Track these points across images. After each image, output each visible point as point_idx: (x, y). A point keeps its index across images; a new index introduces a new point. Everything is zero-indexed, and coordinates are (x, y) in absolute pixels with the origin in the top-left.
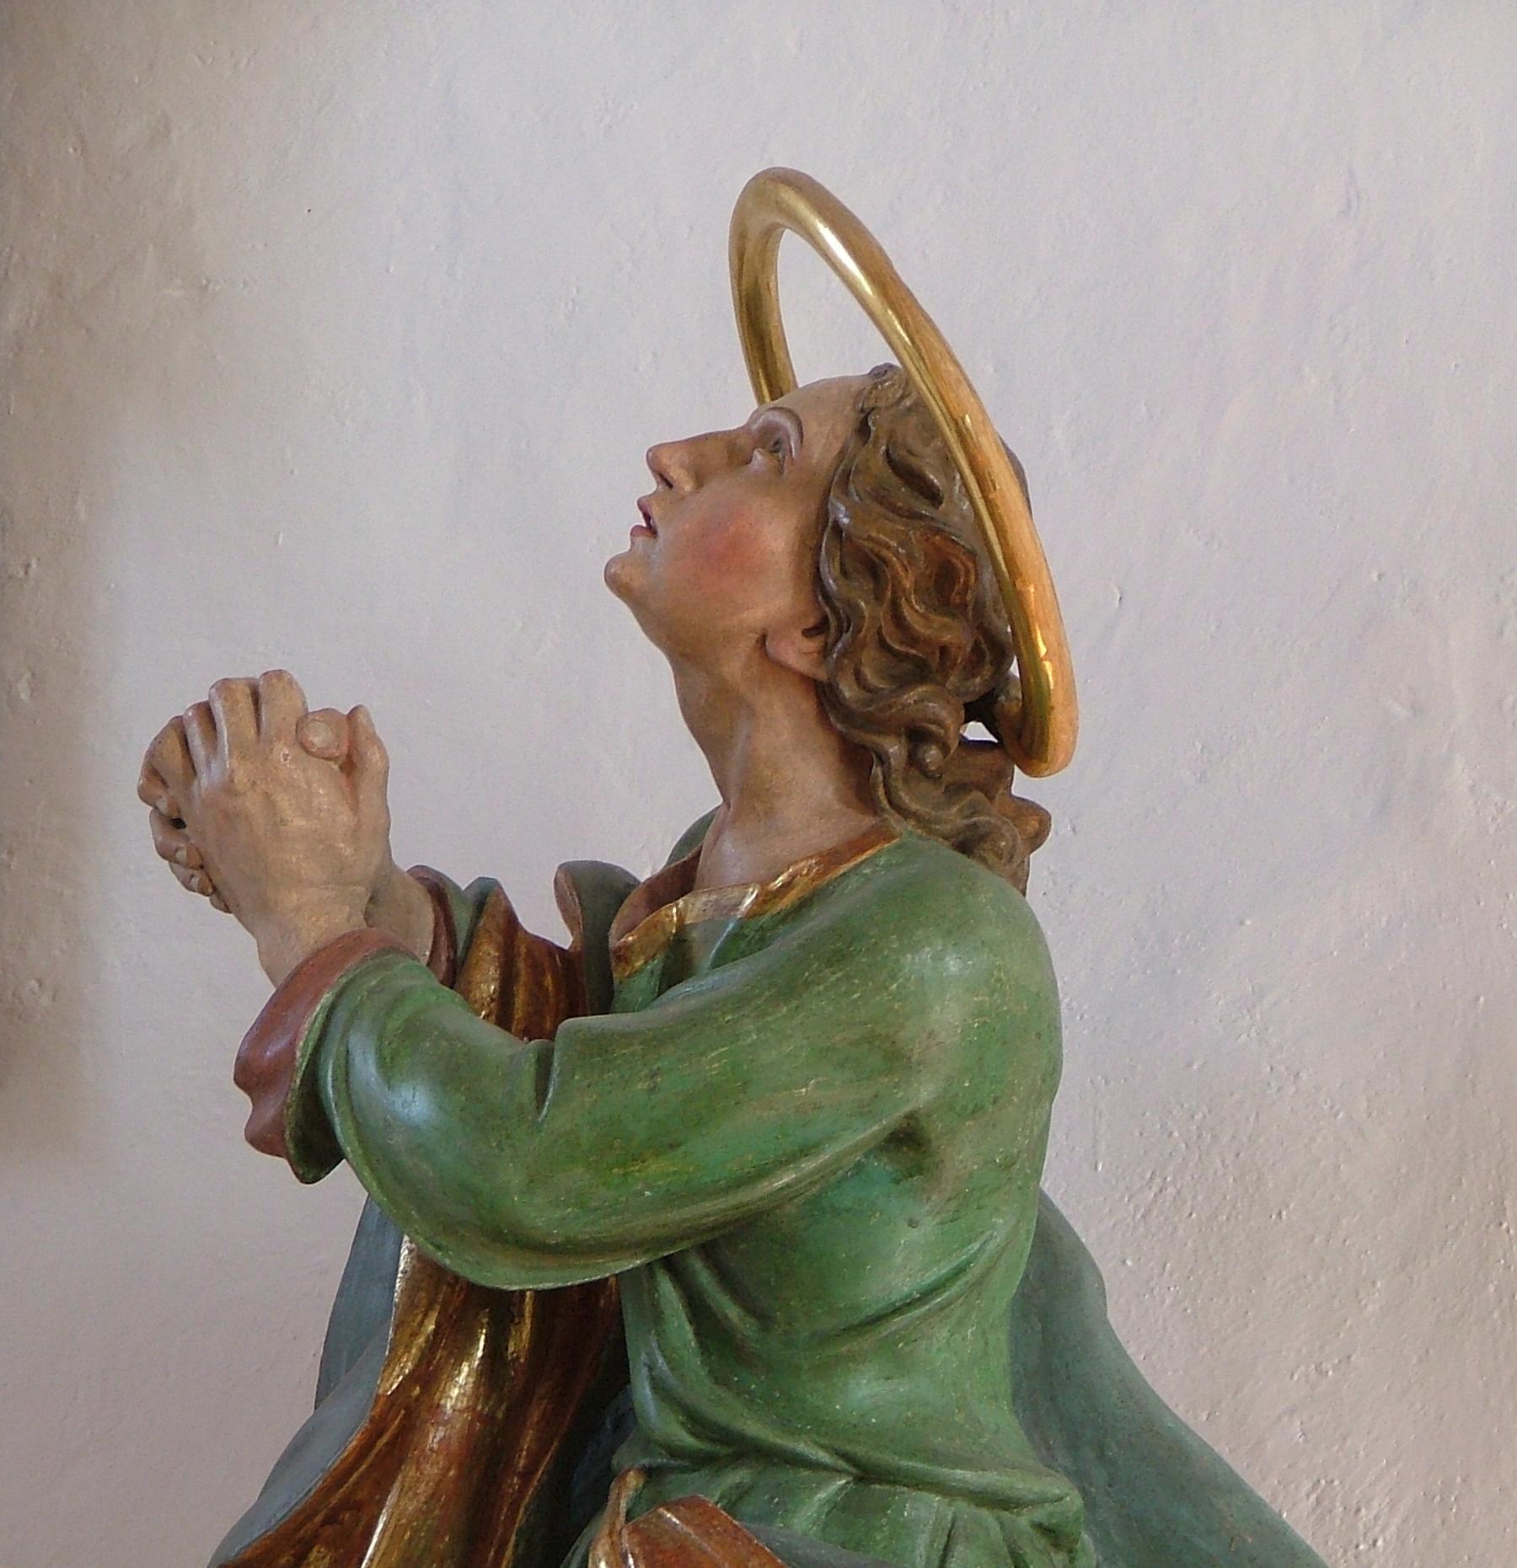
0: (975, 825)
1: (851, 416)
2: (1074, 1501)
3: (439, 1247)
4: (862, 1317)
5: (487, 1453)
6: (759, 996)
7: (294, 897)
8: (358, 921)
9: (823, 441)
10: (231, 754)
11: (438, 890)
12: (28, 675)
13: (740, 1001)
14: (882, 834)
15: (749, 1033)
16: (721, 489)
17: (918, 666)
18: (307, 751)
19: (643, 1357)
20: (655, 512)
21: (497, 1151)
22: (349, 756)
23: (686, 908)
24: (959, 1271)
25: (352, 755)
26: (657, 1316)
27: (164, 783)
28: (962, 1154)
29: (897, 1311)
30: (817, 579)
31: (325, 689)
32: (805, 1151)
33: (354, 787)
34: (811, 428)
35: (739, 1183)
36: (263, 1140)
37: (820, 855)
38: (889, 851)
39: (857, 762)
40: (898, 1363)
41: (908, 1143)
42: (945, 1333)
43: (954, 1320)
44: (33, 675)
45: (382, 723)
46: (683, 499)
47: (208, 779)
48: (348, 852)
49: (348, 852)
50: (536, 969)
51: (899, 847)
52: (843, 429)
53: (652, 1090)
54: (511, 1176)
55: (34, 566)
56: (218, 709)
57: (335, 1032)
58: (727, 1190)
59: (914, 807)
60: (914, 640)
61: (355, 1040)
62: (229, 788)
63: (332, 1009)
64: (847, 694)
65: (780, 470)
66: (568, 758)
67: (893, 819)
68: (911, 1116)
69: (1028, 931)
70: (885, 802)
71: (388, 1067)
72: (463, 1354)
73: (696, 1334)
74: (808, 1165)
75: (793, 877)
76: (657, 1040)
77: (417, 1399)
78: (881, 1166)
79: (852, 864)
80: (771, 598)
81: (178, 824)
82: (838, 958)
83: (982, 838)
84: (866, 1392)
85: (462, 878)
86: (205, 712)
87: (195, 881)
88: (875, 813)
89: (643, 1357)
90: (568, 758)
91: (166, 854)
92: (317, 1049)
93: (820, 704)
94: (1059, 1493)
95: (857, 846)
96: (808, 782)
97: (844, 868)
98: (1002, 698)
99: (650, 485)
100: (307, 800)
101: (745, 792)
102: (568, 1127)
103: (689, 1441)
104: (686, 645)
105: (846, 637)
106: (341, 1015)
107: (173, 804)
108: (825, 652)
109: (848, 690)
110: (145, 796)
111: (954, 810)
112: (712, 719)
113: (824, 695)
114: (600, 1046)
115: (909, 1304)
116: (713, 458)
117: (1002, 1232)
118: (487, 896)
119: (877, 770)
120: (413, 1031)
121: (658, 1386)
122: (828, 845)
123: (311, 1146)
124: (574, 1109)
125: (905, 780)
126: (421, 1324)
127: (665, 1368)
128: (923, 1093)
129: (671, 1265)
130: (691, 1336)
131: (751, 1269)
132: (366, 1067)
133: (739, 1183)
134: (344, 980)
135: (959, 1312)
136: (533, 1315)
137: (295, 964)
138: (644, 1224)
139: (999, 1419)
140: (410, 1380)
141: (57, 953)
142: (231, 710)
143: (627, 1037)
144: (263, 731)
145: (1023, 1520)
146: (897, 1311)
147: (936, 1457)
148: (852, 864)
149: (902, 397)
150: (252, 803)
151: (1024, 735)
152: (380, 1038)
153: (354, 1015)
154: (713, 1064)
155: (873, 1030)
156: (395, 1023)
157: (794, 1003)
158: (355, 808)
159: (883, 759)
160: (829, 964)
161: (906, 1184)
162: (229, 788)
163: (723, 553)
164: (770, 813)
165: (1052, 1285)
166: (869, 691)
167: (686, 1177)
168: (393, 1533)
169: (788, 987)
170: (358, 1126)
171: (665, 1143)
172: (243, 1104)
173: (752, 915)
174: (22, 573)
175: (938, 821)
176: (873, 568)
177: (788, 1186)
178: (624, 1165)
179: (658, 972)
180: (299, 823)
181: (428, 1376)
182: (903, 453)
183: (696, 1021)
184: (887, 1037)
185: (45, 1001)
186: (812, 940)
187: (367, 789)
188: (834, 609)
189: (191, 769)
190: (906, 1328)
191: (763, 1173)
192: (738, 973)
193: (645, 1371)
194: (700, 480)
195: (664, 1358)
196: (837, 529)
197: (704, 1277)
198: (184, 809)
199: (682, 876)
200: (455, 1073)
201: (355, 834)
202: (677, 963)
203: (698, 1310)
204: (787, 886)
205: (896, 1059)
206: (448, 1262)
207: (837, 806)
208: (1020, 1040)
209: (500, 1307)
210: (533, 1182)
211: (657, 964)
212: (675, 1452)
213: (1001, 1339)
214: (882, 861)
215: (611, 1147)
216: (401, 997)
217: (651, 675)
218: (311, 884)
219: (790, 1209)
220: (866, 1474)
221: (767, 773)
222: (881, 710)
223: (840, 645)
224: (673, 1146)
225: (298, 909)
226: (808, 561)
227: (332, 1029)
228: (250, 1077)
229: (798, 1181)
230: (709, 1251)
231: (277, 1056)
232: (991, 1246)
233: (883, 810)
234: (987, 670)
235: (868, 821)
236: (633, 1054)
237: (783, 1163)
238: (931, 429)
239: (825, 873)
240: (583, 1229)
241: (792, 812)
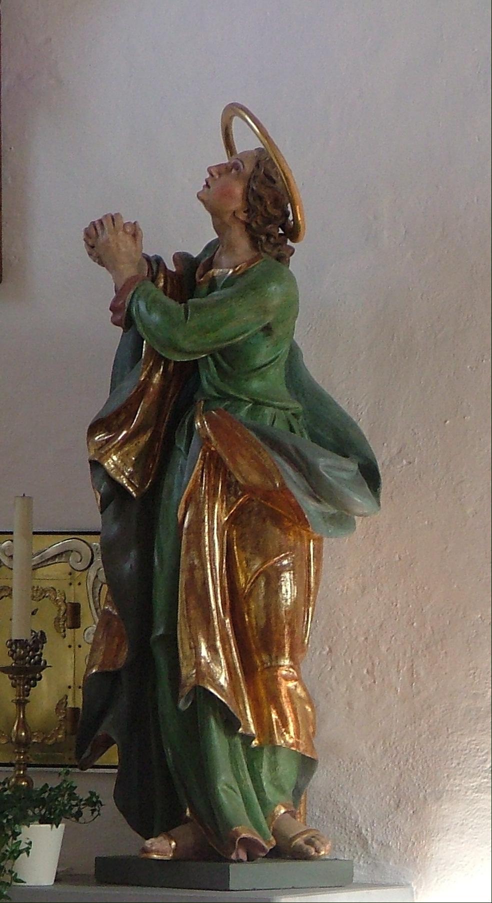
1: (255, 161)
2: (301, 409)
5: (163, 391)
9: (248, 168)
11: (148, 259)
17: (269, 220)
20: (210, 183)
24: (277, 357)
25: (135, 234)
26: (208, 368)
28: (279, 332)
30: (247, 200)
39: (254, 241)
40: (263, 377)
41: (268, 330)
45: (141, 225)
47: (102, 239)
50: (172, 280)
52: (253, 165)
54: (179, 336)
57: (135, 300)
60: (269, 213)
61: (140, 302)
66: (183, 229)
69: (292, 278)
71: (149, 310)
78: (262, 334)
80: (236, 204)
84: (256, 385)
86: (101, 221)
91: (90, 255)
92: (131, 302)
94: (296, 406)
96: (242, 245)
99: (208, 176)
100: (125, 244)
103: (216, 394)
104: (215, 214)
106: (136, 296)
108: (248, 217)
109: (254, 225)
113: (248, 226)
115: (265, 365)
116: (223, 170)
117: (285, 348)
118: (159, 261)
120: (154, 301)
124: (194, 322)
128: (269, 319)
131: (233, 359)
132: (143, 308)
138: (209, 347)
139: (283, 389)
140: (146, 376)
145: (289, 412)
147: (273, 400)
151: (293, 233)
159: (261, 241)
162: (108, 241)
163: (226, 193)
165: (294, 353)
168: (142, 412)
176: (260, 198)
180: (124, 250)
181: (150, 376)
183: (220, 303)
186: (247, 284)
187: (138, 238)
192: (229, 291)
194: (220, 176)
195: (208, 377)
197: (219, 357)
200: (166, 312)
201: (136, 251)
202: (213, 285)
203: (217, 364)
205: (266, 312)
208: (290, 306)
209: (167, 362)
212: (210, 396)
220: (256, 403)
238: (274, 166)
241: (239, 251)
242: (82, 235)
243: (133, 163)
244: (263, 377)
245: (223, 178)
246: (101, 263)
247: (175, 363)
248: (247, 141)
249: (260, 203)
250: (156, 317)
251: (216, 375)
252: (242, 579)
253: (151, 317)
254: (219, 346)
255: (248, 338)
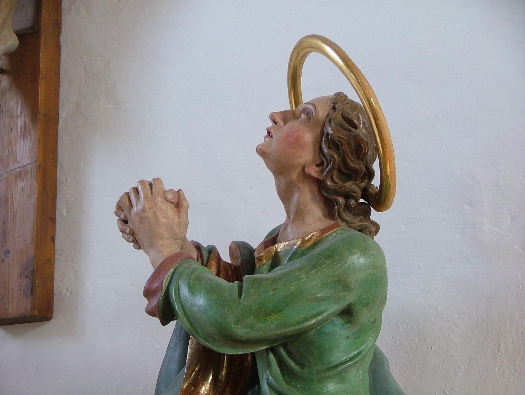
0: (362, 225)
1: (330, 105)
3: (207, 341)
4: (332, 365)
6: (306, 268)
7: (161, 242)
8: (179, 250)
10: (144, 200)
11: (198, 247)
12: (66, 208)
13: (300, 269)
14: (338, 225)
15: (303, 278)
16: (292, 125)
18: (166, 200)
19: (265, 377)
20: (272, 131)
21: (227, 312)
22: (178, 203)
23: (278, 247)
24: (360, 353)
25: (178, 203)
27: (123, 210)
28: (363, 316)
29: (342, 364)
30: (321, 149)
31: (170, 184)
32: (319, 314)
33: (179, 212)
34: (319, 108)
35: (299, 323)
36: (151, 313)
37: (320, 230)
38: (340, 230)
42: (355, 371)
43: (357, 367)
44: (68, 208)
45: (188, 195)
46: (281, 127)
48: (177, 230)
49: (177, 230)
50: (226, 269)
51: (343, 229)
53: (274, 295)
54: (231, 319)
55: (69, 179)
56: (140, 188)
58: (295, 325)
59: (346, 218)
61: (180, 282)
62: (143, 210)
63: (173, 274)
64: (329, 183)
65: (309, 119)
66: (242, 205)
67: (339, 221)
68: (349, 305)
70: (337, 216)
71: (192, 289)
72: (206, 379)
73: (281, 370)
74: (319, 318)
75: (312, 236)
76: (274, 280)
77: (193, 391)
78: (338, 321)
79: (329, 233)
80: (306, 156)
81: (126, 222)
82: (329, 257)
83: (366, 228)
85: (205, 244)
86: (136, 190)
87: (131, 239)
88: (334, 220)
89: (265, 377)
90: (242, 205)
91: (123, 231)
93: (319, 188)
95: (331, 228)
97: (327, 234)
98: (370, 189)
99: (270, 124)
101: (296, 215)
102: (249, 305)
105: (330, 166)
106: (176, 275)
107: (125, 216)
108: (322, 171)
110: (117, 214)
111: (357, 220)
112: (285, 194)
113: (320, 184)
114: (258, 281)
116: (286, 117)
118: (212, 250)
119: (336, 207)
120: (199, 279)
121: (269, 385)
122: (321, 228)
123: (165, 312)
125: (344, 211)
126: (195, 368)
127: (272, 380)
128: (350, 298)
129: (273, 350)
130: (279, 371)
132: (184, 291)
133: (299, 323)
134: (177, 265)
135: (359, 365)
136: (227, 367)
137: (161, 262)
141: (72, 282)
142: (144, 188)
143: (266, 279)
144: (153, 192)
146: (342, 364)
148: (329, 233)
149: (345, 100)
150: (150, 214)
152: (189, 280)
153: (180, 275)
154: (293, 287)
155: (340, 278)
156: (193, 277)
157: (316, 270)
158: (179, 218)
160: (327, 258)
161: (345, 326)
164: (303, 219)
166: (335, 183)
167: (283, 321)
169: (315, 265)
170: (182, 306)
171: (277, 310)
172: (145, 301)
173: (300, 247)
174: (65, 181)
175: (352, 223)
177: (314, 324)
178: (265, 317)
179: (270, 265)
180: (163, 220)
182: (346, 114)
184: (344, 280)
185: (68, 295)
187: (182, 213)
188: (326, 159)
189: (131, 206)
190: (345, 369)
191: (306, 320)
192: (298, 263)
193: (265, 381)
194: (285, 122)
196: (328, 134)
197: (284, 353)
198: (128, 217)
199: (273, 239)
200: (212, 290)
201: (179, 225)
202: (276, 261)
204: (310, 238)
206: (210, 345)
207: (323, 218)
210: (238, 321)
211: (269, 262)
213: (367, 374)
214: (339, 232)
215: (262, 311)
216: (194, 270)
217: (268, 181)
218: (166, 238)
219: (311, 333)
221: (303, 207)
222: (339, 188)
223: (327, 169)
224: (280, 311)
225: (162, 246)
226: (318, 146)
227: (174, 279)
228: (148, 293)
229: (317, 322)
230: (285, 346)
231: (157, 286)
232: (369, 346)
233: (337, 219)
234: (366, 181)
235: (332, 222)
236: (268, 284)
237: (315, 316)
239: (321, 235)
240: (252, 334)
241: (309, 219)
242: (113, 208)
243: (184, 133)
244: (341, 378)
245: (290, 124)
246: (138, 244)
247: (227, 355)
248: (322, 82)
249: (339, 163)
250: (200, 301)
251: (281, 378)
252: (299, 243)
253: (196, 301)
254: (284, 331)
255: (320, 323)
